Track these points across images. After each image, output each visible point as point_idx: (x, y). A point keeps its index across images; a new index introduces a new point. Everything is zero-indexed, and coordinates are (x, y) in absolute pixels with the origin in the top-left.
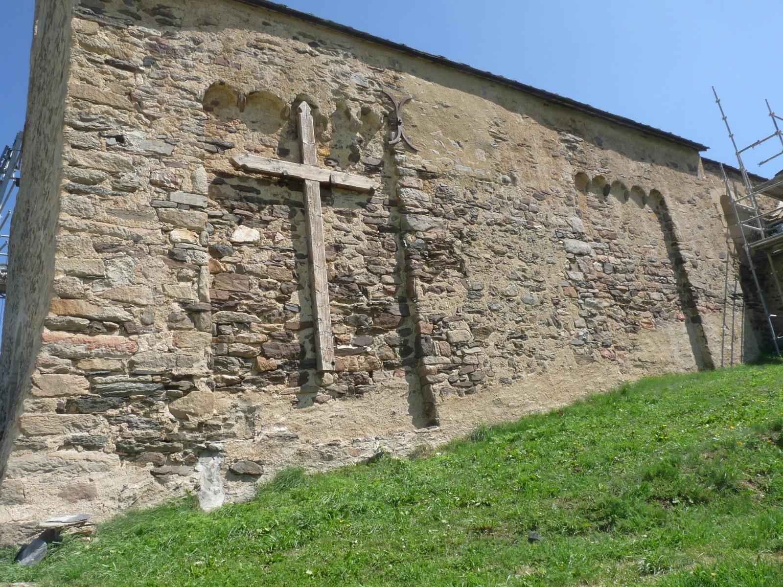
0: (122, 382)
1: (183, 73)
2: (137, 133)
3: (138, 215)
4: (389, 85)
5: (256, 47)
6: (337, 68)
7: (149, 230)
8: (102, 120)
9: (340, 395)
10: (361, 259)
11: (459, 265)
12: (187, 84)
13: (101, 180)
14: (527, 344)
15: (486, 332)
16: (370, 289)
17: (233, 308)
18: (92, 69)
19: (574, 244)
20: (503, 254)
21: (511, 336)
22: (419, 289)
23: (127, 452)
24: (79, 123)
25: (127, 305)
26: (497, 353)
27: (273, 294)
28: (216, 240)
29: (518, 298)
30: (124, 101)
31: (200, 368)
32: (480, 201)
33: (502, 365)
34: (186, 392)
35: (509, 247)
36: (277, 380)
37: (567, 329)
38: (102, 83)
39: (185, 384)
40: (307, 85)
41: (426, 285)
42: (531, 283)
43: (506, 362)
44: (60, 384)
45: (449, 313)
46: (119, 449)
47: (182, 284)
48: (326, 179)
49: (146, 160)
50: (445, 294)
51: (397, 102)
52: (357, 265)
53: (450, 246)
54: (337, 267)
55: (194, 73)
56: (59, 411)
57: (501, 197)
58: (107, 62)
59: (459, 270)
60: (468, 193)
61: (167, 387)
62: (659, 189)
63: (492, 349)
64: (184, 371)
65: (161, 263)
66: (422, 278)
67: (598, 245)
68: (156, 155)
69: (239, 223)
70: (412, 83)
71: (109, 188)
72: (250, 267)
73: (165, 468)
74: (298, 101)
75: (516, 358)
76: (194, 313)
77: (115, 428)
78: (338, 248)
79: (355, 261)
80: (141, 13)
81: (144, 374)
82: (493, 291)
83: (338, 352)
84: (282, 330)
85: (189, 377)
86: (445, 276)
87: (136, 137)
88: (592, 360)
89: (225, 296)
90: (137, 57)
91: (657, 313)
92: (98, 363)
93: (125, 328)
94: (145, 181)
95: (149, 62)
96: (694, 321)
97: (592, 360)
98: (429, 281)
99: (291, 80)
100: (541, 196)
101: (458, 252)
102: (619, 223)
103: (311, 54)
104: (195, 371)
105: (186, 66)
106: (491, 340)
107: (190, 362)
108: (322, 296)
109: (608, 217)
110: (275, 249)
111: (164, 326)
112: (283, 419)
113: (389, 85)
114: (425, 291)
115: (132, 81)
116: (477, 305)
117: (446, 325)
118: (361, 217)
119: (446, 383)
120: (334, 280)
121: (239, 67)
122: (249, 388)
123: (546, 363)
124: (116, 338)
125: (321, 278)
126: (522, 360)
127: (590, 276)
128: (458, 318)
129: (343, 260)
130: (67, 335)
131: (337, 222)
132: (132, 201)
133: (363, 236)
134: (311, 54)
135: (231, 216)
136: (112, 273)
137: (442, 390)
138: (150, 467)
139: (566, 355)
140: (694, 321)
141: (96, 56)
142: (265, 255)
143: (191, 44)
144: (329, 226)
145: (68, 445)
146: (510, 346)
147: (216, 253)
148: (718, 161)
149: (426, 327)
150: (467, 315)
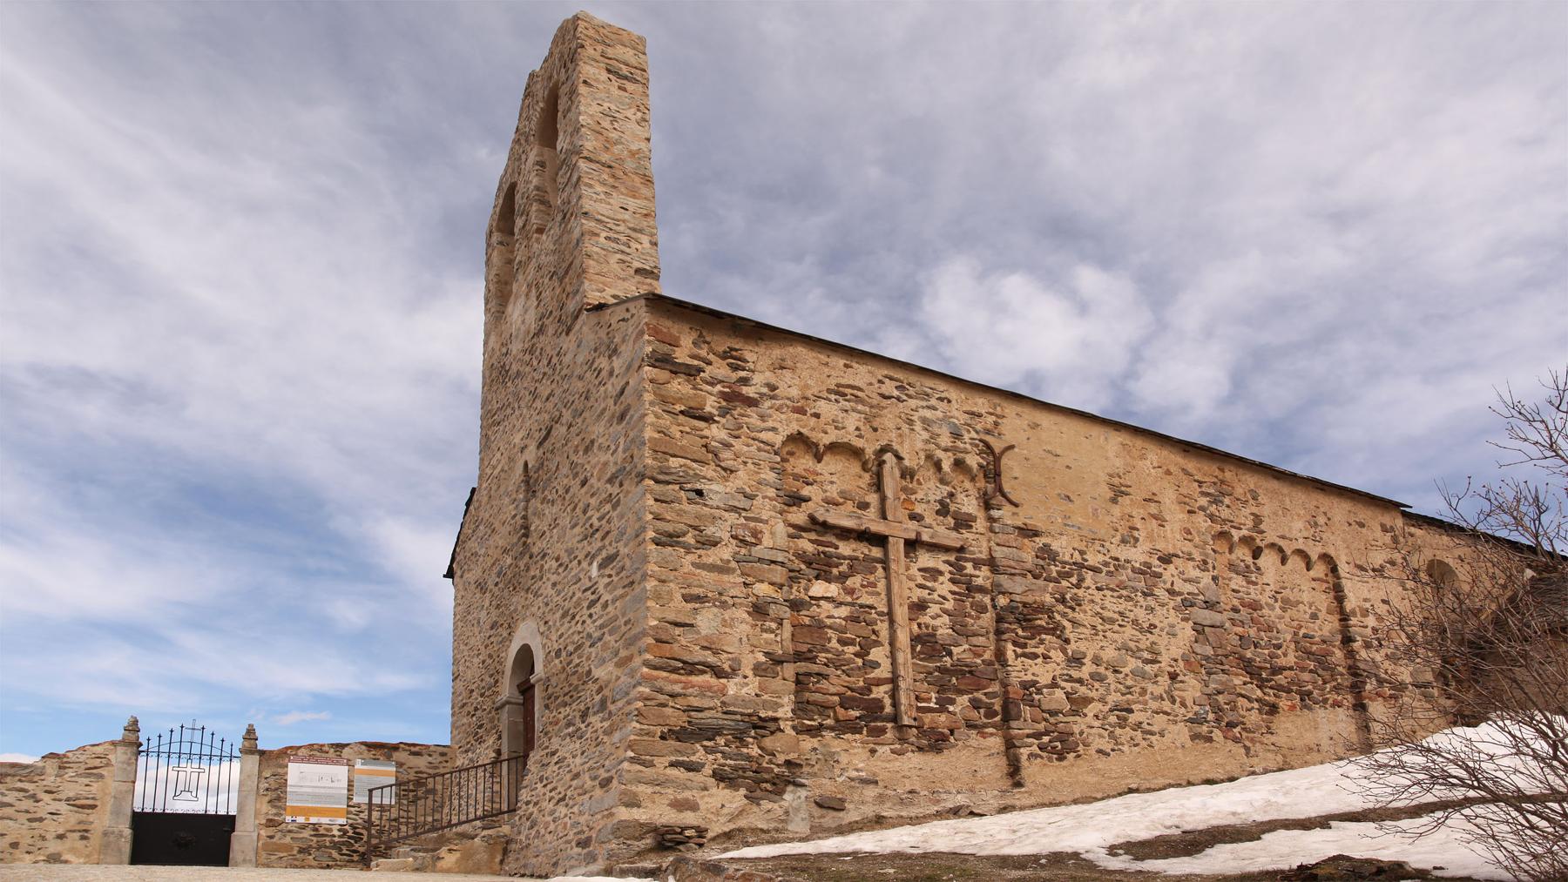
0: (710, 718)
1: (759, 423)
2: (715, 487)
3: (722, 569)
4: (988, 432)
5: (837, 393)
6: (928, 414)
7: (732, 583)
8: (1479, 821)
9: (920, 749)
10: (946, 619)
11: (1055, 629)
12: (764, 436)
13: (684, 534)
14: (1132, 718)
15: (1087, 701)
16: (955, 650)
17: (813, 660)
18: (667, 420)
19: (1206, 616)
20: (1112, 621)
21: (1116, 708)
22: (1010, 654)
23: (720, 776)
24: (661, 477)
26: (1097, 723)
27: (851, 649)
28: (794, 594)
29: (1126, 670)
30: (702, 454)
31: (785, 711)
32: (1090, 563)
33: (1101, 736)
34: (772, 733)
35: (1121, 614)
36: (856, 730)
37: (1183, 704)
38: (678, 435)
39: (772, 726)
40: (893, 435)
41: (1019, 651)
42: (1146, 655)
43: (1106, 734)
44: (662, 716)
45: (1045, 679)
46: (715, 774)
47: (765, 635)
48: (913, 536)
49: (726, 515)
50: (1040, 660)
51: (997, 451)
53: (1049, 611)
54: (919, 625)
55: (770, 424)
56: (663, 738)
57: (1117, 559)
58: (682, 412)
59: (1059, 637)
60: (1076, 554)
61: (755, 727)
62: (1333, 554)
63: (1090, 719)
64: (770, 714)
65: (746, 616)
66: (1015, 644)
67: (1236, 616)
68: (734, 509)
69: (817, 578)
71: (692, 541)
72: (829, 622)
73: (758, 793)
74: (884, 450)
75: (1118, 731)
77: (711, 757)
78: (919, 607)
79: (937, 622)
80: (711, 357)
81: (734, 713)
82: (1097, 661)
83: (919, 709)
84: (861, 684)
85: (776, 720)
86: (1042, 642)
87: (718, 491)
88: (1210, 740)
89: (804, 648)
90: (711, 405)
91: (1305, 696)
92: (696, 702)
93: (718, 673)
94: (726, 536)
96: (1360, 707)
97: (1210, 740)
98: (1024, 646)
99: (875, 430)
100: (1166, 560)
101: (1058, 617)
102: (1268, 592)
103: (898, 399)
104: (779, 714)
105: (762, 418)
106: (1091, 710)
107: (777, 706)
108: (904, 656)
109: (1255, 584)
110: (852, 604)
111: (750, 674)
112: (861, 765)
113: (988, 432)
114: (1017, 656)
115: (706, 432)
116: (1075, 674)
117: (1039, 692)
118: (948, 576)
119: (1035, 749)
120: (916, 639)
121: (817, 416)
122: (829, 735)
123: (1153, 738)
124: (707, 678)
125: (903, 638)
126: (1124, 734)
127: (1220, 651)
130: (665, 674)
131: (920, 581)
132: (713, 556)
133: (950, 596)
134: (898, 399)
135: (808, 571)
137: (1031, 755)
138: (743, 791)
139: (1181, 732)
140: (1360, 707)
141: (670, 407)
142: (844, 611)
143: (765, 390)
144: (912, 584)
145: (672, 765)
146: (1113, 719)
150: (1063, 684)
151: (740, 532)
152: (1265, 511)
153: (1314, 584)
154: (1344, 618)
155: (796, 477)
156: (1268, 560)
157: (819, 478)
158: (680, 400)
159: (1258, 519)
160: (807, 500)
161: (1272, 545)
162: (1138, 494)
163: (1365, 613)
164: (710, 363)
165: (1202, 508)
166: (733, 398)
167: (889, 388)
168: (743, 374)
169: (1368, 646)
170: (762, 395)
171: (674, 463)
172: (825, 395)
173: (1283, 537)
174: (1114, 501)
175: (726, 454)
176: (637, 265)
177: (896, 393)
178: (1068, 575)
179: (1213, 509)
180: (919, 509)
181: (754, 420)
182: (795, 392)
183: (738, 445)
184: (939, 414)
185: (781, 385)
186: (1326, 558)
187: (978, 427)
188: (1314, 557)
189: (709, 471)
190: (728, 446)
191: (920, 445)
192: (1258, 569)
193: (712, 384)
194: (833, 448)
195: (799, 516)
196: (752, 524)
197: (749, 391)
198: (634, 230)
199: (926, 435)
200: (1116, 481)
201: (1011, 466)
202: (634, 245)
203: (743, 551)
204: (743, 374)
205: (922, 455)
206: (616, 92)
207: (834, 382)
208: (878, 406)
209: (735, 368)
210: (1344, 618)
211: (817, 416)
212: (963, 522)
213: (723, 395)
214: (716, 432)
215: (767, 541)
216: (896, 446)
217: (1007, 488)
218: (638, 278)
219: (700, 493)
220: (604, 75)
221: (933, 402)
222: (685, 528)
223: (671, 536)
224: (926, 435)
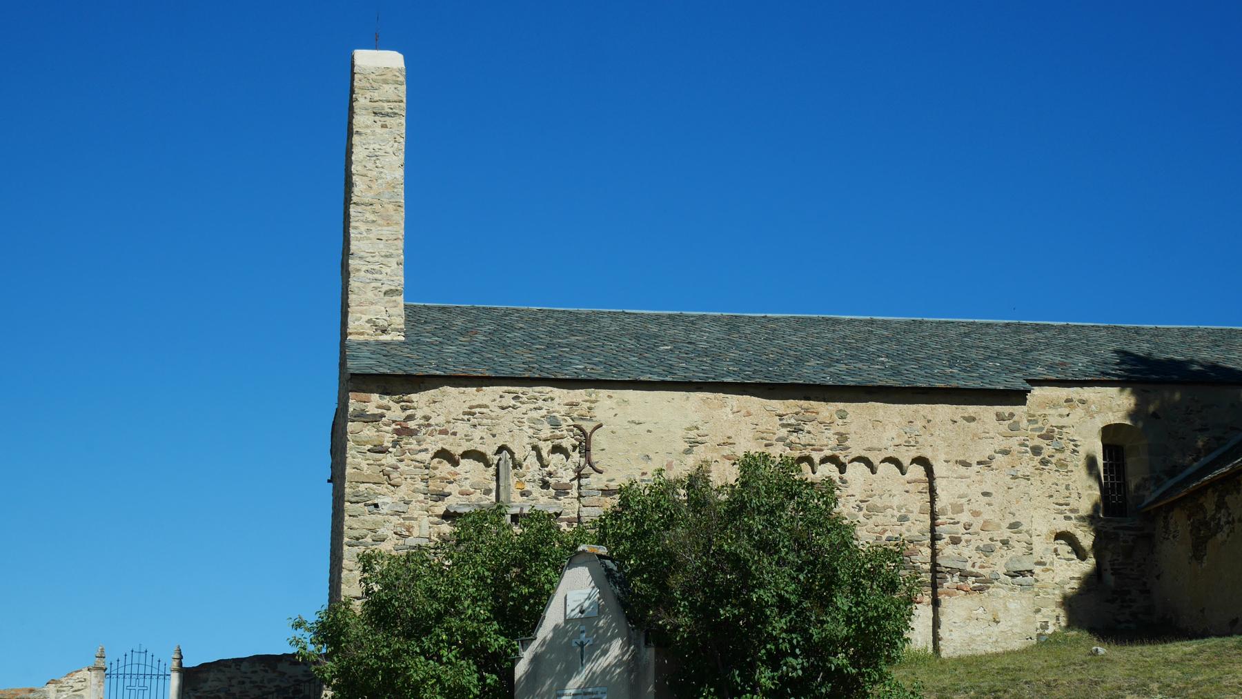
2: (386, 500)
4: (582, 417)
5: (470, 413)
40: (507, 437)
49: (392, 518)
51: (588, 431)
55: (423, 447)
71: (370, 540)
90: (387, 441)
94: (390, 534)
95: (395, 444)
99: (494, 436)
105: (419, 443)
115: (383, 462)
121: (454, 434)
143: (422, 422)
151: (399, 530)
152: (851, 428)
153: (908, 487)
154: (934, 516)
155: (442, 479)
156: (856, 472)
157: (457, 477)
158: (366, 443)
159: (842, 437)
160: (450, 494)
161: (860, 459)
162: (711, 441)
163: (958, 509)
164: (389, 409)
165: (780, 439)
166: (403, 431)
167: (509, 400)
168: (409, 412)
169: (955, 541)
170: (420, 426)
171: (362, 487)
172: (461, 416)
173: (869, 449)
174: (688, 452)
175: (394, 475)
176: (385, 288)
177: (513, 402)
179: (793, 437)
180: (528, 487)
181: (414, 446)
182: (442, 419)
183: (402, 466)
184: (544, 412)
185: (433, 415)
186: (921, 461)
187: (575, 415)
188: (906, 461)
189: (382, 489)
190: (396, 468)
191: (527, 440)
192: (844, 482)
193: (389, 425)
194: (467, 455)
195: (441, 508)
196: (407, 522)
197: (412, 425)
198: (386, 256)
199: (531, 432)
200: (693, 434)
201: (598, 439)
202: (385, 270)
203: (401, 542)
204: (409, 412)
205: (529, 448)
206: (379, 130)
207: (468, 404)
208: (497, 417)
209: (404, 409)
210: (934, 516)
211: (454, 434)
212: (562, 491)
213: (397, 432)
214: (389, 460)
215: (416, 533)
216: (509, 445)
217: (594, 458)
218: (387, 298)
219: (376, 506)
220: (372, 117)
221: (540, 403)
222: (365, 531)
223: (358, 539)
224: (531, 432)
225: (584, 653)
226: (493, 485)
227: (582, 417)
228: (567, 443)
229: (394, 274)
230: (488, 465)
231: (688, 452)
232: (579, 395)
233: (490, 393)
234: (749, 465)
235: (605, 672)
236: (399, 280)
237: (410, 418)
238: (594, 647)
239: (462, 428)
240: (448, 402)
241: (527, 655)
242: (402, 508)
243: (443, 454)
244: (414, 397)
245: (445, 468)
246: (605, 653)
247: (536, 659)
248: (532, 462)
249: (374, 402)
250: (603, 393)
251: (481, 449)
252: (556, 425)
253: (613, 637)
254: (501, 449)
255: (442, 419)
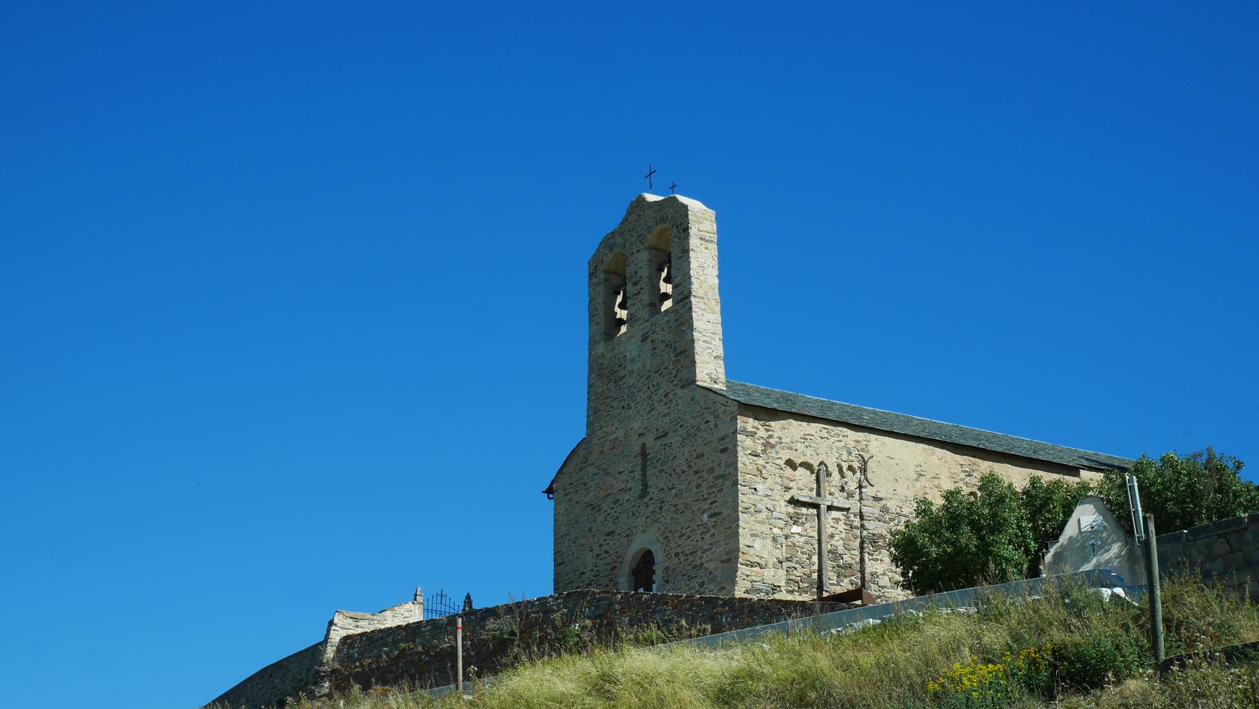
3: (762, 522)
25: (761, 558)
31: (782, 583)
45: (880, 571)
52: (838, 544)
70: (877, 444)
76: (781, 562)
90: (759, 449)
95: (764, 451)
128: (884, 574)
129: (833, 542)
136: (756, 545)
142: (803, 539)
147: (786, 537)
148: (491, 606)
149: (868, 577)
155: (788, 478)
167: (824, 434)
174: (917, 480)
178: (891, 520)
179: (967, 479)
181: (774, 455)
182: (788, 440)
197: (772, 441)
200: (919, 469)
214: (760, 461)
217: (869, 477)
225: (1094, 550)
226: (815, 486)
227: (863, 450)
228: (856, 465)
229: (719, 349)
230: (812, 472)
231: (917, 480)
232: (861, 436)
233: (815, 428)
234: (950, 496)
235: (1107, 562)
236: (720, 352)
237: (770, 437)
238: (1101, 547)
239: (800, 447)
240: (792, 429)
241: (1052, 551)
242: (769, 493)
243: (790, 464)
244: (772, 423)
245: (789, 471)
246: (1108, 551)
247: (1056, 555)
248: (836, 474)
249: (750, 423)
250: (873, 437)
251: (811, 462)
252: (850, 453)
253: (1113, 542)
254: (822, 463)
255: (788, 440)
